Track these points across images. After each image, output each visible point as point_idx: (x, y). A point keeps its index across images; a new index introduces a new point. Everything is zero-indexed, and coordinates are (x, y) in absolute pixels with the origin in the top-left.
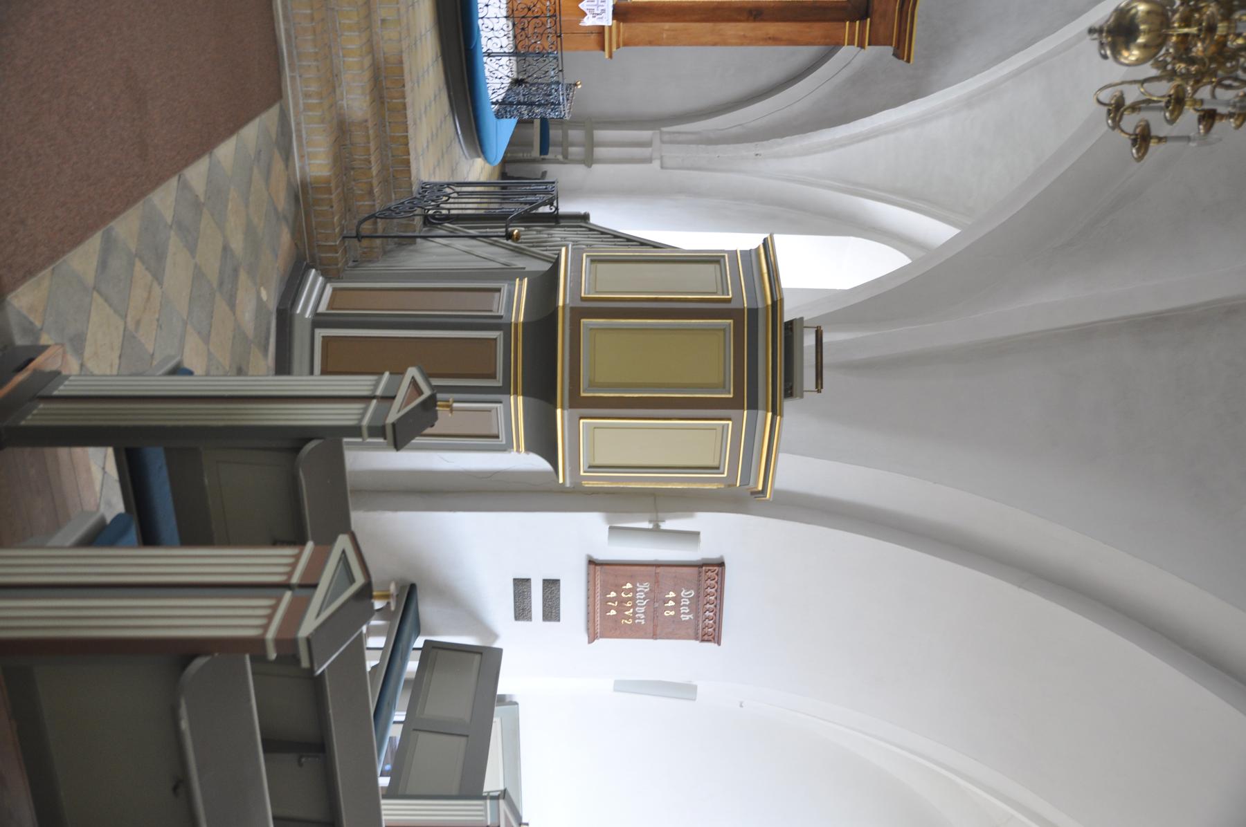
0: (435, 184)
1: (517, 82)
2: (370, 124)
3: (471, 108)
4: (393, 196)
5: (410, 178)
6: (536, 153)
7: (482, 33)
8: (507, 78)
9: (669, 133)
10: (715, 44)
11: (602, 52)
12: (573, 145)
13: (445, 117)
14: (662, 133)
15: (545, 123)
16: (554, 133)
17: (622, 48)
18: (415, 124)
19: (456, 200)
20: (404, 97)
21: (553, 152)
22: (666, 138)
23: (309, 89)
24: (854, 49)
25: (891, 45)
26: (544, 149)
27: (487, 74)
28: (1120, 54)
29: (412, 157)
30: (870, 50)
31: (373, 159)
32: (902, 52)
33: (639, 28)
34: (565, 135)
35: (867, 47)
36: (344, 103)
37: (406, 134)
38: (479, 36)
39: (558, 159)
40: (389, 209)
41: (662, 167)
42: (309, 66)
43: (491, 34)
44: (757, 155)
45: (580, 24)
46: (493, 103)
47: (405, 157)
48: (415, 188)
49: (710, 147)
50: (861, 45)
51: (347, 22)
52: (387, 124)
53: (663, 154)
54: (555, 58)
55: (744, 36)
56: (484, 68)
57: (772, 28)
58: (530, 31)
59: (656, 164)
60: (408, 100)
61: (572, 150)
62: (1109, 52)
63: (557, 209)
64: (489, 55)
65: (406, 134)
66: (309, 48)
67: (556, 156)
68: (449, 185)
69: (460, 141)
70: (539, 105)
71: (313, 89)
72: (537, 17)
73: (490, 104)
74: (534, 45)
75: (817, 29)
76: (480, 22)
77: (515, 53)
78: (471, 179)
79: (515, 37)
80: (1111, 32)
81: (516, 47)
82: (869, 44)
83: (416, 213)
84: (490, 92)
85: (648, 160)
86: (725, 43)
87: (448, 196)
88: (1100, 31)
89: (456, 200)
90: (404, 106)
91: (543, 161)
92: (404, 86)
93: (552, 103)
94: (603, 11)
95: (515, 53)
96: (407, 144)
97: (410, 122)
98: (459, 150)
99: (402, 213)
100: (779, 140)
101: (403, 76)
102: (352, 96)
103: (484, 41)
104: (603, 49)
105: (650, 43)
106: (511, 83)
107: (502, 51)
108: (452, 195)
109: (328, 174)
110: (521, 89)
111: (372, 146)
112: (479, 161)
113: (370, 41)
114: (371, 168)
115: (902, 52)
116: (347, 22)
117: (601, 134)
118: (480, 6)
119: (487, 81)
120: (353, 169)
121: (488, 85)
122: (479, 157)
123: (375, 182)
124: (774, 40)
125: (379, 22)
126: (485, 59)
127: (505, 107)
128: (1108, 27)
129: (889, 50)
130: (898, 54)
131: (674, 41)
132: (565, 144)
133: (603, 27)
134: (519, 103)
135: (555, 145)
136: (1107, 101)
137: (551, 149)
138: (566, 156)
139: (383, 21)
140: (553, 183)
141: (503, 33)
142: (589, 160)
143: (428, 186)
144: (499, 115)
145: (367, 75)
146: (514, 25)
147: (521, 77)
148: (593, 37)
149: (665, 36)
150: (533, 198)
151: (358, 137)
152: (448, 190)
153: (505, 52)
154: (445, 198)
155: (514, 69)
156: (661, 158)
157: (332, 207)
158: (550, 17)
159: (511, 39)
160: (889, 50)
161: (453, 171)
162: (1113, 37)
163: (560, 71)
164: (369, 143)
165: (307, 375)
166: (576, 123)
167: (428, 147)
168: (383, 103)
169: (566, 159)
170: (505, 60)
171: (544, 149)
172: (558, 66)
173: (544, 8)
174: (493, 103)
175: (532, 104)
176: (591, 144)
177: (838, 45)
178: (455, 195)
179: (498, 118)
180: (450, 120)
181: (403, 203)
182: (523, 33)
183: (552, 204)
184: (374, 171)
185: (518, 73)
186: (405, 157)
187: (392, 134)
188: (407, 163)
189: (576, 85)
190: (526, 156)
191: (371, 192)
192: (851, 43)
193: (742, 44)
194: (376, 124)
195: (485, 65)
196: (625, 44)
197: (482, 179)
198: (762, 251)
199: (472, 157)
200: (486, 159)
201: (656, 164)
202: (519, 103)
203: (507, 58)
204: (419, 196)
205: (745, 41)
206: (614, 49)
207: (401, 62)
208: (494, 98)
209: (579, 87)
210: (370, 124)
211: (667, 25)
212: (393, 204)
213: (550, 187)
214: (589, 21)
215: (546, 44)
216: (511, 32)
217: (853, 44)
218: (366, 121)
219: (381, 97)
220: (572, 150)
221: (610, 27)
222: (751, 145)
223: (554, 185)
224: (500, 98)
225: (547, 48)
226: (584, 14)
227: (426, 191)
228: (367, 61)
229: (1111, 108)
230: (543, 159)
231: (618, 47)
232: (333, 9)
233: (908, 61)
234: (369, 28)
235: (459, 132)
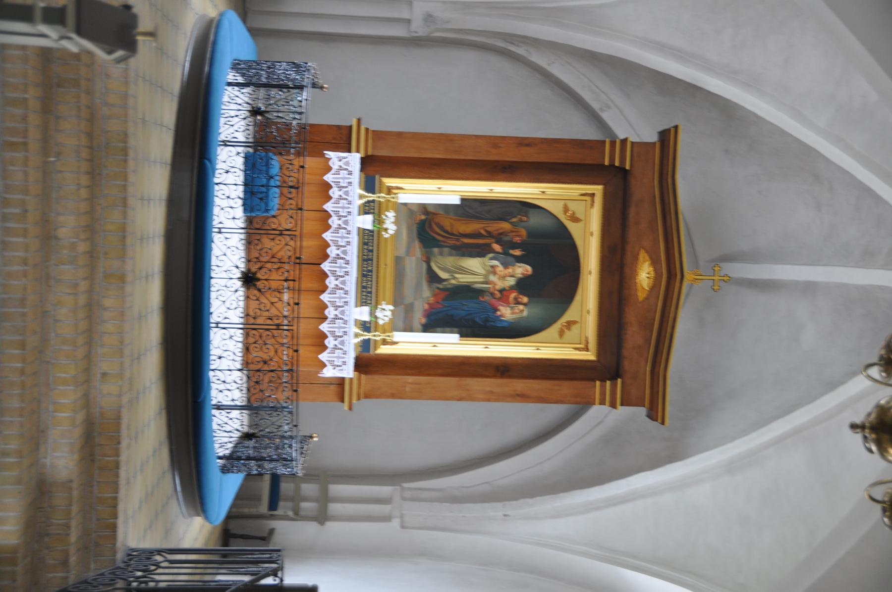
0: (144, 551)
1: (247, 436)
2: (75, 485)
3: (193, 463)
4: (93, 566)
5: (114, 544)
6: (264, 508)
7: (212, 385)
8: (236, 432)
9: (410, 489)
10: (460, 399)
11: (341, 404)
12: (305, 499)
13: (164, 473)
14: (403, 489)
15: (276, 479)
16: (286, 487)
17: (363, 401)
18: (128, 483)
19: (167, 571)
20: (117, 455)
21: (284, 508)
22: (407, 494)
23: (8, 446)
24: (606, 408)
25: (644, 406)
26: (273, 505)
27: (215, 426)
28: (887, 452)
29: (120, 521)
30: (623, 411)
31: (73, 523)
32: (655, 412)
33: (381, 381)
34: (298, 489)
35: (620, 408)
36: (48, 461)
37: (115, 495)
38: (209, 388)
39: (287, 516)
40: (85, 582)
41: (403, 527)
42: (12, 422)
43: (222, 387)
44: (505, 515)
45: (320, 375)
46: (220, 458)
47: (112, 521)
48: (120, 556)
49: (455, 506)
50: (613, 405)
51: (62, 375)
52: (95, 483)
53: (404, 512)
54: (291, 413)
55: (491, 392)
56: (211, 421)
57: (520, 385)
58: (264, 386)
59: (396, 523)
60: (123, 458)
61: (305, 505)
62: (874, 448)
63: (282, 580)
64: (219, 407)
65: (115, 495)
66: (15, 403)
67: (285, 512)
68: (160, 552)
69: (178, 499)
70: (272, 460)
71: (12, 447)
72: (272, 371)
73: (215, 458)
74: (269, 398)
75: (566, 388)
76: (211, 374)
77: (248, 407)
78: (186, 545)
79: (248, 390)
80: (874, 428)
81: (249, 400)
82: (622, 405)
83: (118, 586)
84: (217, 446)
85: (387, 519)
86: (470, 398)
87: (158, 565)
88: (862, 427)
89: (167, 571)
90: (117, 465)
91: (272, 517)
92: (119, 443)
93: (285, 459)
94: (344, 363)
95: (248, 407)
96: (115, 506)
97: (122, 482)
98: (177, 508)
99: (101, 587)
100: (529, 501)
101: (119, 432)
102: (57, 454)
103: (214, 393)
104: (342, 400)
105: (393, 396)
106: (241, 437)
107: (232, 403)
108: (163, 565)
109: (16, 542)
110: (252, 443)
111: (75, 508)
112: (198, 521)
113: (86, 396)
114: (68, 535)
115: (655, 412)
116: (62, 375)
117: (336, 489)
118: (212, 358)
119: (215, 434)
120: (48, 535)
121: (215, 439)
122: (198, 515)
123: (72, 550)
124: (522, 397)
125: (99, 376)
126: (214, 412)
127: (232, 461)
128: (870, 423)
129: (642, 411)
130: (652, 415)
131: (418, 394)
132: (297, 498)
133: (343, 379)
134: (249, 458)
135: (287, 499)
136: (879, 498)
137: (281, 504)
138: (297, 512)
139: (104, 375)
140: (279, 551)
141: (235, 386)
142: (322, 517)
143: (135, 553)
144: (225, 470)
145: (78, 432)
146: (248, 377)
147: (252, 431)
148: (333, 387)
149: (408, 389)
150: (255, 569)
151: (59, 500)
152: (159, 558)
153: (236, 406)
154: (153, 568)
155: (246, 422)
156: (402, 516)
157: (14, 581)
158: (287, 371)
159: (244, 392)
160: (642, 411)
161: (167, 532)
162: (876, 433)
163: (295, 426)
164: (70, 505)
165: (372, 339)
166: (311, 476)
167: (140, 508)
168: (93, 461)
169: (298, 516)
170: (235, 413)
171: (273, 504)
172: (292, 420)
173: (281, 361)
174: (220, 458)
175: (262, 459)
176: (325, 499)
177: (589, 403)
178: (166, 564)
179: (223, 472)
180: (169, 476)
181: (102, 574)
182: (257, 386)
183: (276, 575)
184: (73, 538)
185: (250, 426)
186: (112, 521)
187: (100, 495)
188: (113, 528)
189: (311, 437)
190: (253, 511)
191: (65, 563)
192: (602, 403)
193: (489, 400)
194: (82, 485)
195: (213, 418)
196: (367, 397)
197: (198, 545)
198: (658, 146)
199: (191, 516)
200: (207, 518)
201: (396, 523)
202: (249, 458)
203: (238, 412)
204: (122, 565)
205: (491, 397)
206: (354, 401)
207: (118, 418)
208: (222, 452)
209: (315, 439)
210: (75, 485)
211: (410, 379)
212: (91, 575)
213: (275, 555)
214: (328, 372)
215: (282, 396)
216: (245, 385)
217: (604, 404)
218: (71, 481)
219: (92, 455)
220: (305, 505)
221: (351, 379)
222: (499, 505)
223: (279, 553)
224: (227, 452)
225: (281, 402)
226: (324, 365)
227: (130, 560)
228: (80, 417)
229: (885, 505)
230: (272, 515)
231: (359, 399)
232: (48, 362)
233: (663, 423)
234: (87, 381)
235: (179, 488)
